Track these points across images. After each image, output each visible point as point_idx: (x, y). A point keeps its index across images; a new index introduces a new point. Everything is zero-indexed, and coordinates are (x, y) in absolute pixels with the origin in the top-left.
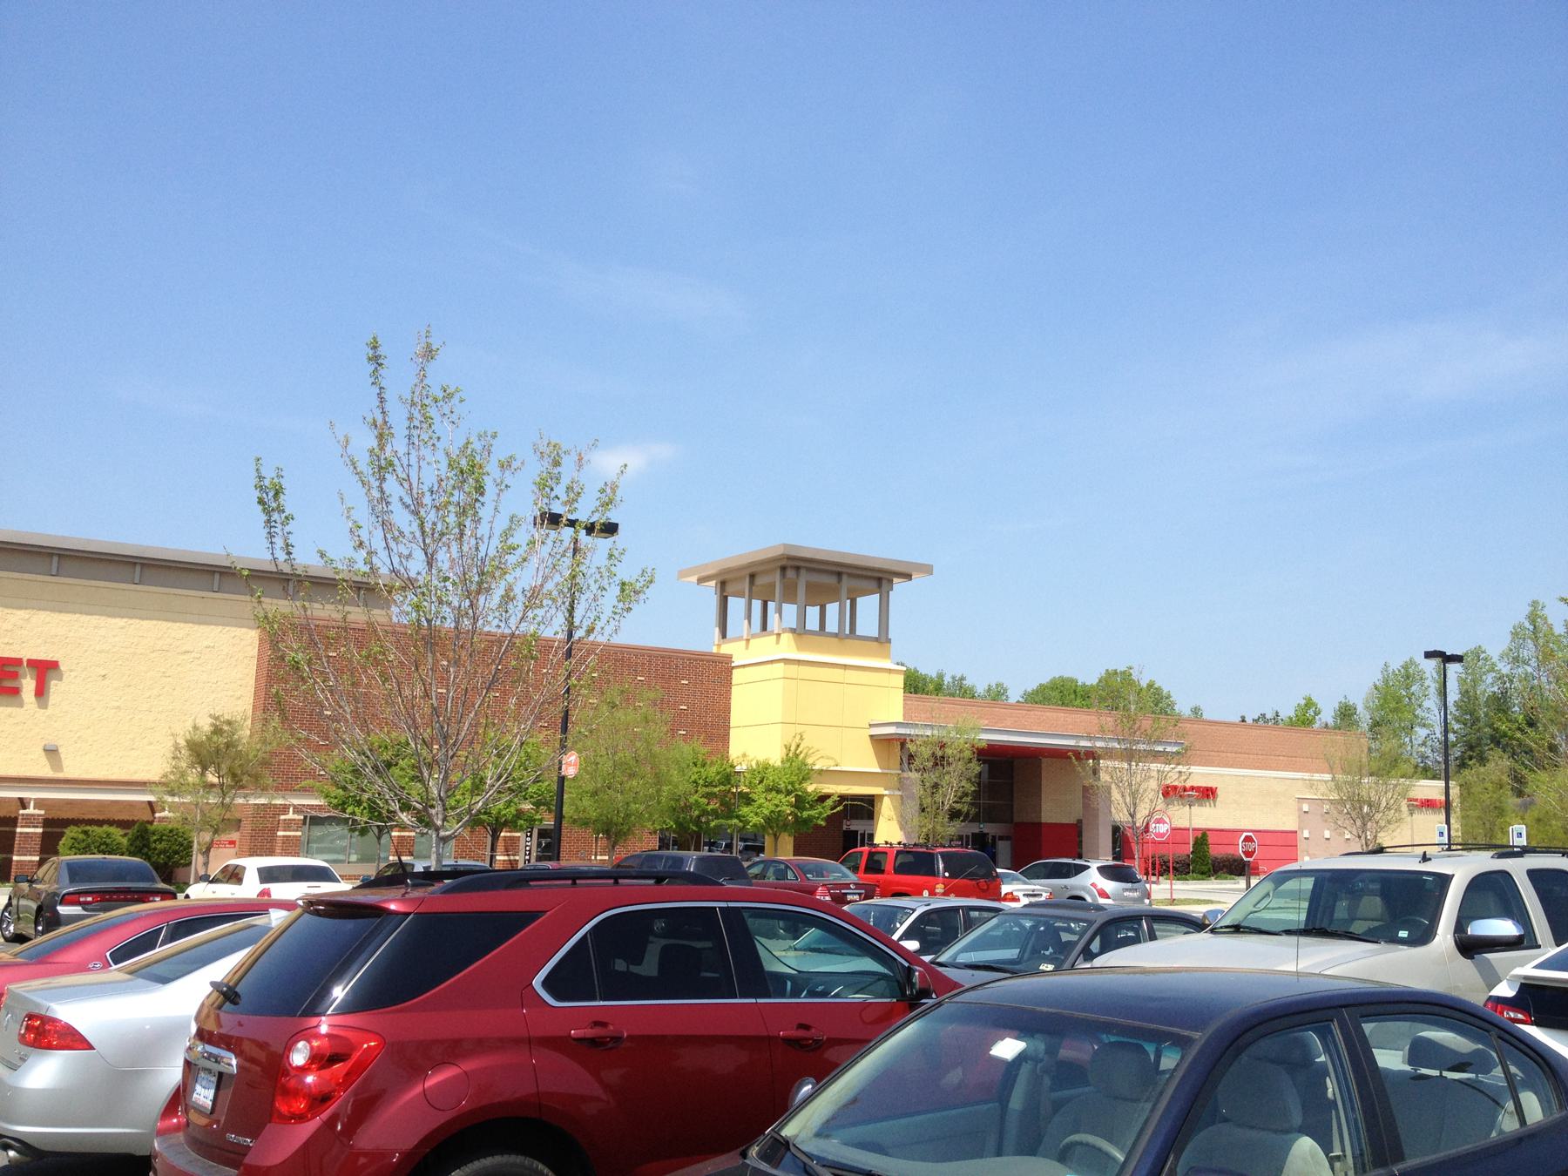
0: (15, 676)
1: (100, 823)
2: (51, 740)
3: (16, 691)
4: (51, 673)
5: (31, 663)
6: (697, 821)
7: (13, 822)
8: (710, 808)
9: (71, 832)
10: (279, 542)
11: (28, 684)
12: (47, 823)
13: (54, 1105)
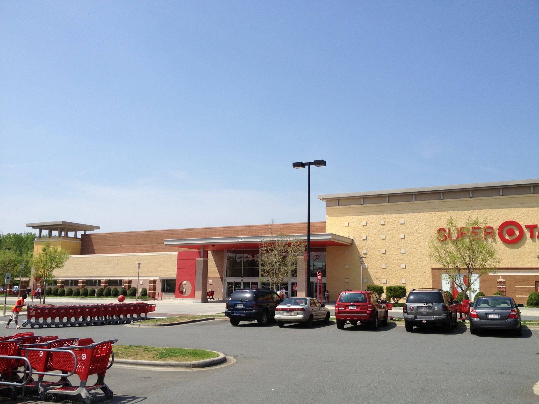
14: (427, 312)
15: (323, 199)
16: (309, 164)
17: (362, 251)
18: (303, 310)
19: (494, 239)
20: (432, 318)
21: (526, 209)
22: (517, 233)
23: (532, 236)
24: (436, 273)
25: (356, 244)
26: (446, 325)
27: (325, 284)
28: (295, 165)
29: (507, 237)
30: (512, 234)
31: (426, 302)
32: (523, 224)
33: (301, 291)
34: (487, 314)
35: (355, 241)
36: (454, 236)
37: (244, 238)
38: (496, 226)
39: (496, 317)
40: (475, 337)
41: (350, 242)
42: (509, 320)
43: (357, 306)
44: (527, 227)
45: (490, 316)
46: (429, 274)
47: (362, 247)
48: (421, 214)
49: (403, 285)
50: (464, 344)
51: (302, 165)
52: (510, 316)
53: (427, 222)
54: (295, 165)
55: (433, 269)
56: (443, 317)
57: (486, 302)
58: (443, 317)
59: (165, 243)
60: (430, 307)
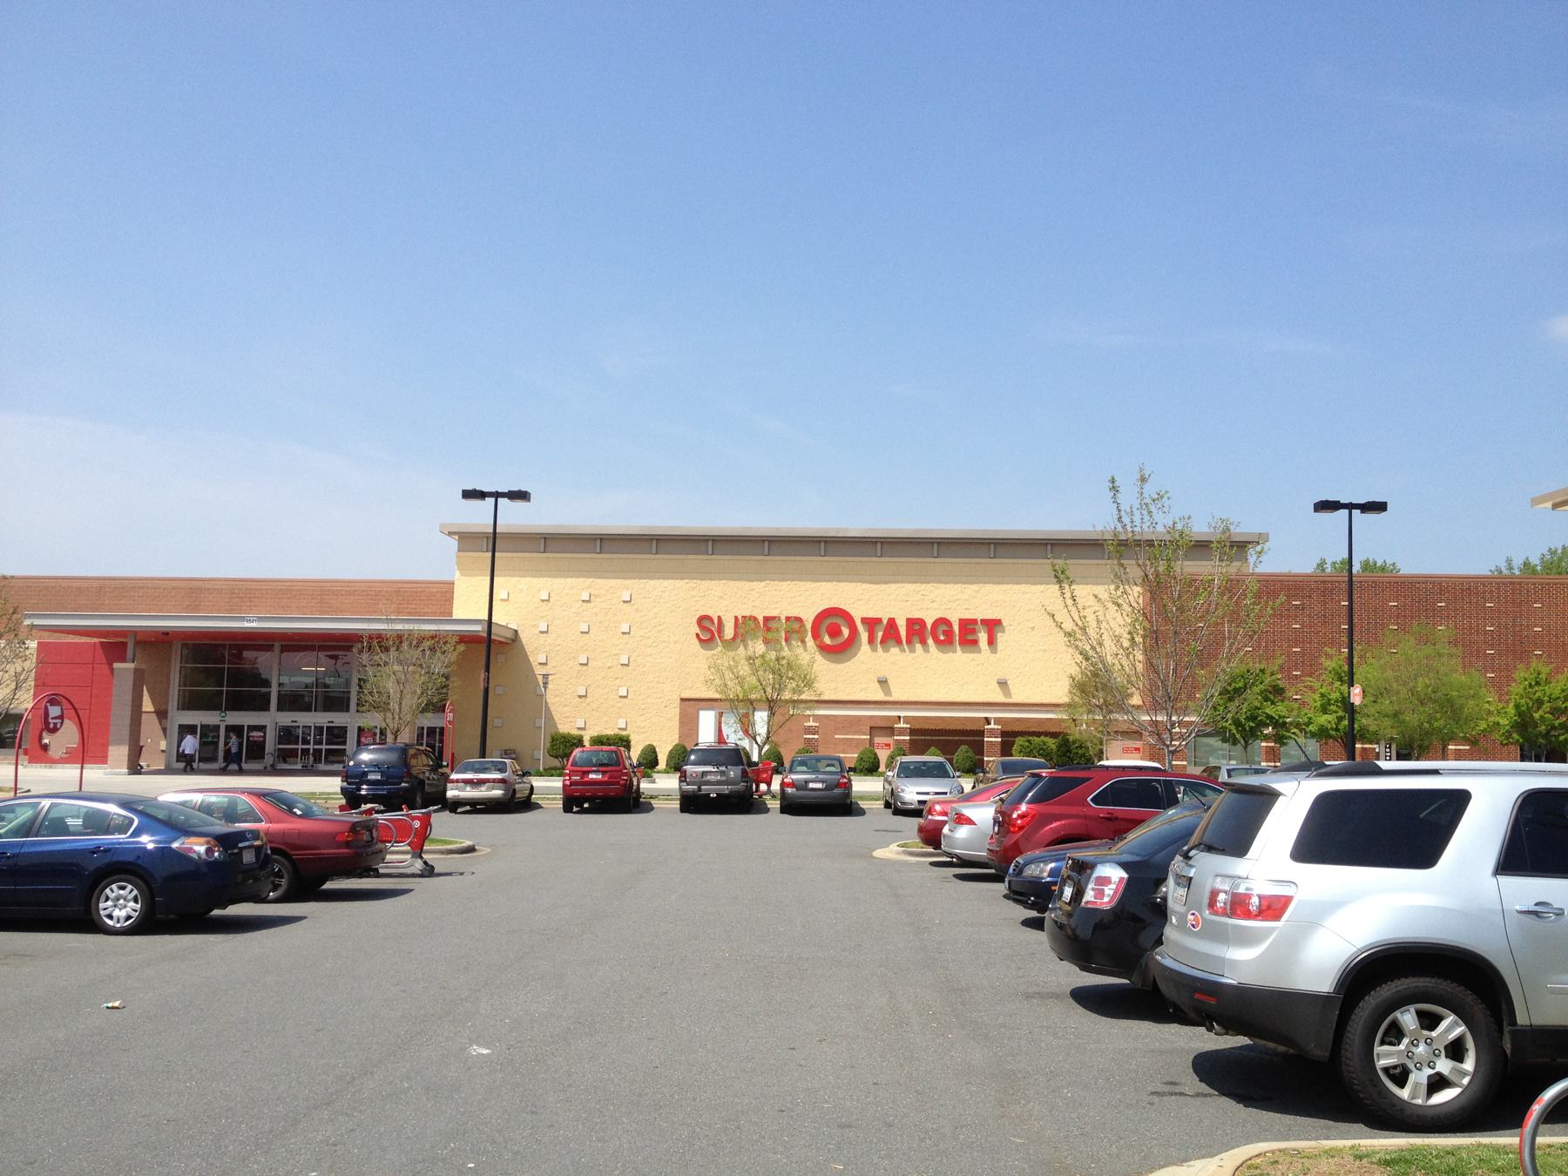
0: (973, 631)
1: (1038, 734)
2: (1001, 676)
3: (975, 642)
4: (996, 628)
5: (984, 622)
6: (1547, 735)
7: (981, 733)
8: (1556, 723)
9: (1020, 741)
10: (1068, 595)
11: (983, 637)
12: (1004, 734)
13: (967, 844)
14: (715, 778)
15: (450, 534)
16: (497, 495)
17: (536, 658)
18: (503, 781)
19: (803, 641)
20: (726, 789)
21: (865, 586)
22: (846, 632)
23: (871, 640)
24: (690, 707)
25: (524, 641)
26: (741, 803)
27: (442, 729)
28: (469, 494)
29: (827, 640)
30: (836, 633)
31: (718, 765)
32: (857, 616)
33: (119, 743)
34: (807, 782)
35: (524, 637)
36: (729, 632)
37: (260, 619)
38: (809, 618)
39: (819, 786)
40: (786, 817)
41: (510, 635)
42: (837, 791)
43: (604, 773)
44: (865, 621)
45: (811, 785)
46: (674, 711)
47: (536, 650)
48: (666, 583)
49: (575, 732)
50: (770, 829)
51: (481, 495)
52: (839, 785)
53: (673, 600)
54: (469, 494)
55: (683, 700)
56: (727, 792)
57: (802, 763)
58: (727, 792)
59: (27, 622)
60: (722, 773)
